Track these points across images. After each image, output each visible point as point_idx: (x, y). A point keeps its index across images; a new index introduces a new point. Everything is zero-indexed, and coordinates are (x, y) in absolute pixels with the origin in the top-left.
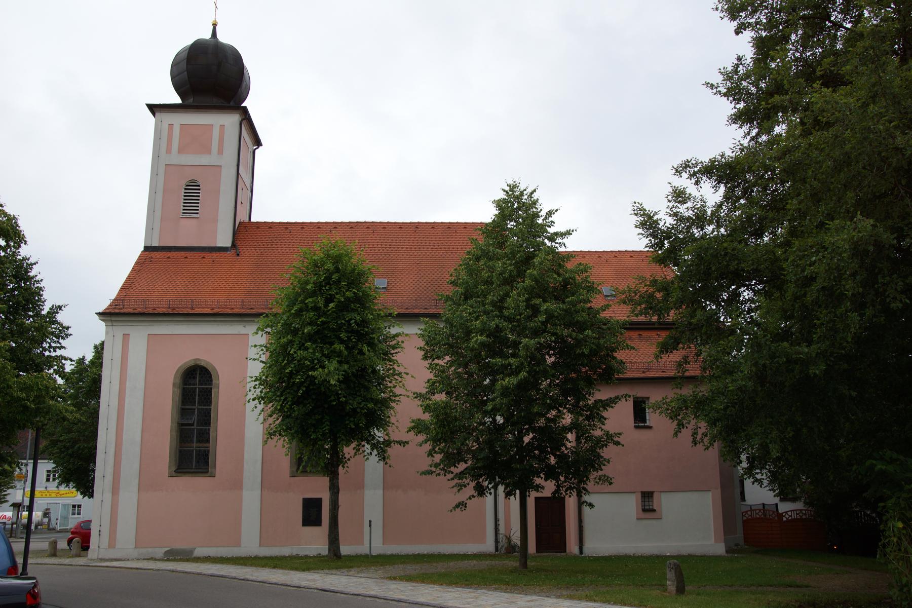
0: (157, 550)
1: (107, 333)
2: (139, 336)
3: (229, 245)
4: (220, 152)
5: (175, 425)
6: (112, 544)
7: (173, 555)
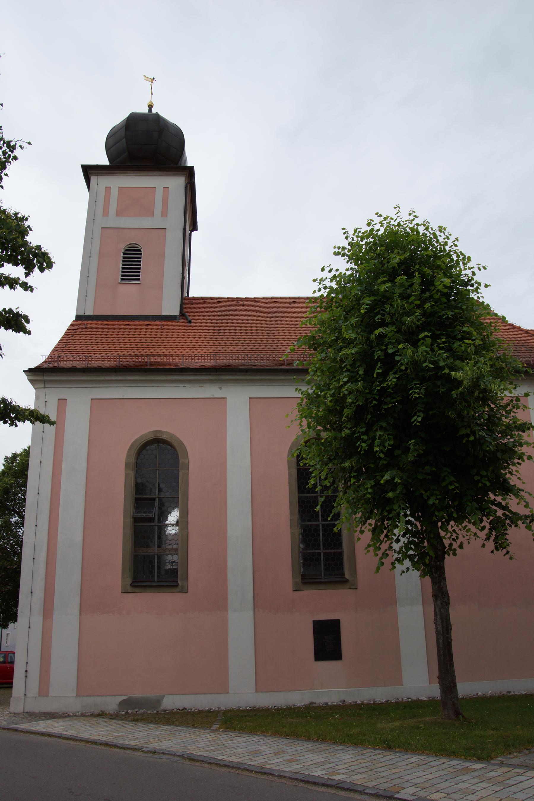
0: (108, 699)
1: (37, 398)
2: (79, 403)
3: (177, 312)
4: (164, 213)
5: (130, 520)
6: (44, 690)
7: (139, 711)
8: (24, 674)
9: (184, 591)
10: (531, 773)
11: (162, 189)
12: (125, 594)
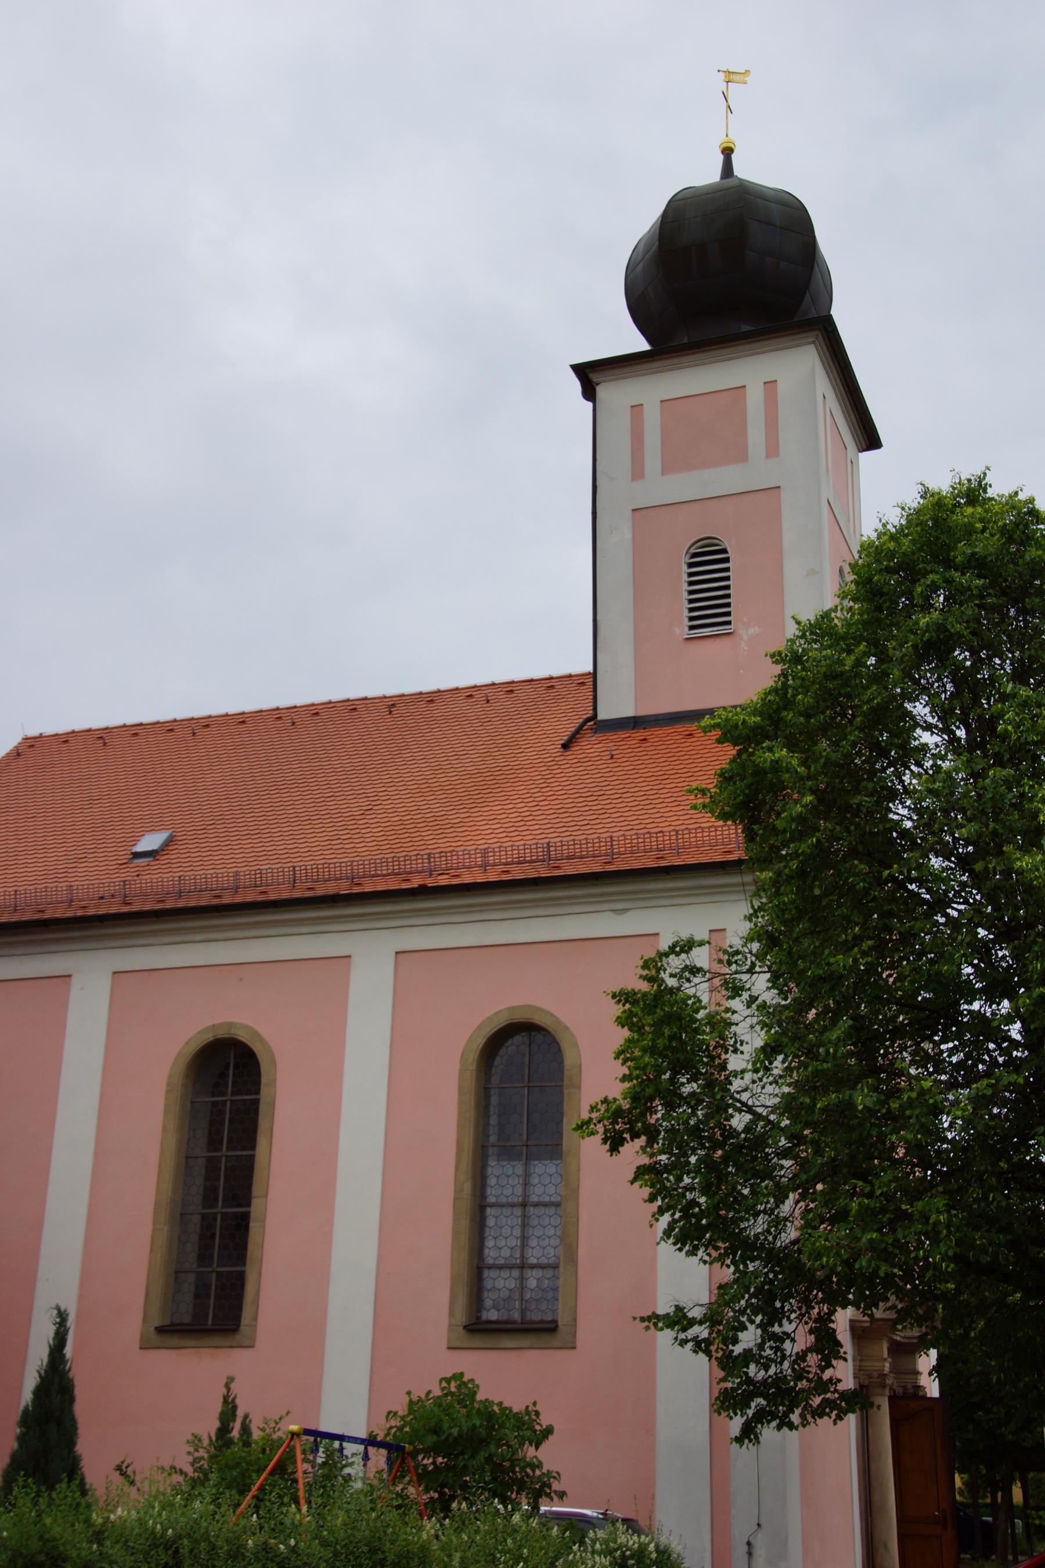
4: (772, 450)
8: (746, 1548)
9: (145, 1346)
10: (4, 919)
11: (761, 388)
12: (454, 1353)
